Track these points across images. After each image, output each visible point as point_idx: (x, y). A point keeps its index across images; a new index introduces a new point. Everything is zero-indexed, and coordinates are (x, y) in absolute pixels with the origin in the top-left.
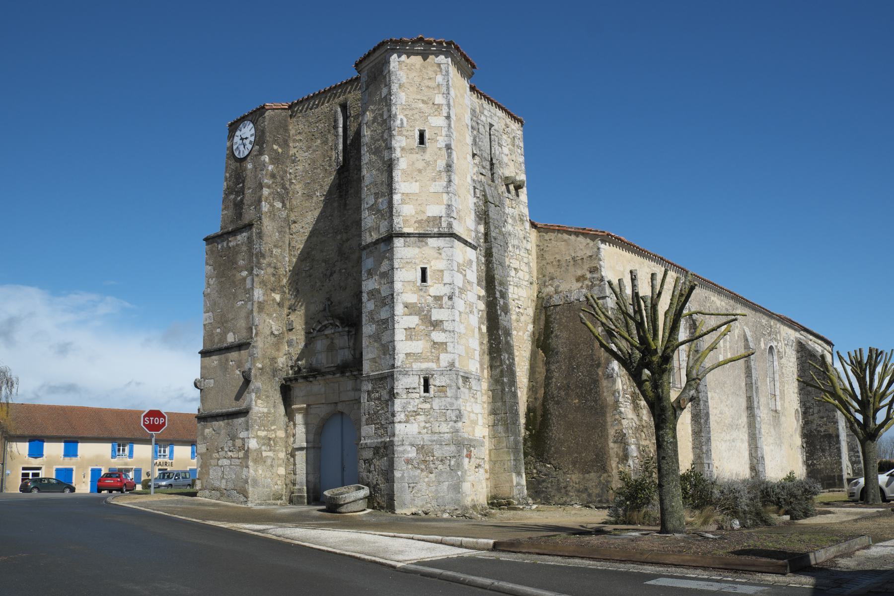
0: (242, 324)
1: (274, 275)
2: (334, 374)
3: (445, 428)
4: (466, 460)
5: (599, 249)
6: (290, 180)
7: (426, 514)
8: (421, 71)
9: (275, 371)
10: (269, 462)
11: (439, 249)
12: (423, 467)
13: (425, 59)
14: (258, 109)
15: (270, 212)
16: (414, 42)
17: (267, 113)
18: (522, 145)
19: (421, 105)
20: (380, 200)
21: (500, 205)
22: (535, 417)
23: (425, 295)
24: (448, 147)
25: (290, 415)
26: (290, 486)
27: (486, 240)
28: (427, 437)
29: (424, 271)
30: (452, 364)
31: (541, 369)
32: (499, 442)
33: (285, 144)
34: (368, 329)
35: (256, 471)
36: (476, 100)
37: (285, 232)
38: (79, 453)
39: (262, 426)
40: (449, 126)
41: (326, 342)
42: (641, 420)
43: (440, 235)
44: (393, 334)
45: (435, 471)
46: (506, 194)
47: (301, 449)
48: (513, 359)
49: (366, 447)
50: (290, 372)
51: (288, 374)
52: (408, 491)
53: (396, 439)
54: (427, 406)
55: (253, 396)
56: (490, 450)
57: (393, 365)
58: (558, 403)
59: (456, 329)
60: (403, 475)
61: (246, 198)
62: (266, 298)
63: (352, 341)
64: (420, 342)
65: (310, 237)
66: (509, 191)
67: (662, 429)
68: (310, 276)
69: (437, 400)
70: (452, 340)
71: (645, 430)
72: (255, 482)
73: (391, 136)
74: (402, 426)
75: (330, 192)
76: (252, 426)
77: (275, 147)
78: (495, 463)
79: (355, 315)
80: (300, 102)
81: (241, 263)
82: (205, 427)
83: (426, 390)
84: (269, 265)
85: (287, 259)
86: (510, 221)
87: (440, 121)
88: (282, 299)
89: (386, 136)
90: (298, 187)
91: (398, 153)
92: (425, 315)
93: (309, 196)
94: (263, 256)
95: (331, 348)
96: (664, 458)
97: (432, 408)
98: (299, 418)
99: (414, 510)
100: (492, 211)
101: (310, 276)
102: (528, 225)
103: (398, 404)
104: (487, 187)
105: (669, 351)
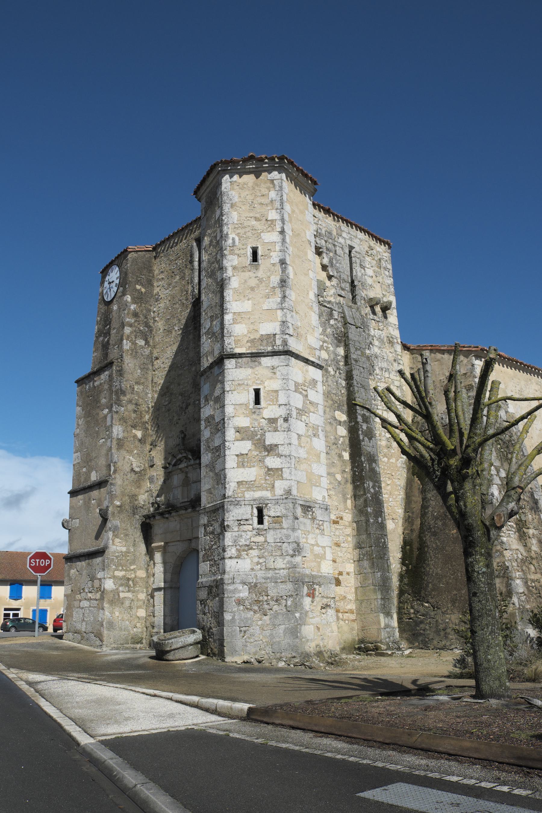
0: (102, 461)
1: (135, 411)
2: (186, 509)
3: (280, 563)
4: (307, 601)
5: (473, 365)
6: (154, 318)
7: (259, 662)
8: (254, 189)
9: (135, 509)
10: (127, 603)
11: (273, 368)
12: (256, 608)
13: (257, 177)
14: (122, 253)
15: (132, 350)
16: (245, 161)
17: (130, 256)
18: (390, 266)
19: (254, 222)
20: (214, 323)
21: (363, 326)
22: (411, 550)
23: (258, 418)
24: (283, 262)
25: (150, 552)
26: (150, 628)
27: (346, 363)
28: (260, 574)
29: (257, 392)
30: (289, 492)
31: (417, 498)
32: (365, 579)
33: (149, 284)
34: (206, 458)
35: (112, 613)
36: (333, 223)
37: (148, 369)
38: (53, 595)
39: (120, 566)
40: (284, 241)
41: (181, 476)
42: (529, 550)
43: (275, 353)
44: (224, 462)
45: (269, 613)
46: (372, 316)
47: (159, 589)
48: (380, 487)
50: (152, 509)
51: (149, 511)
52: (239, 636)
53: (226, 576)
54: (261, 539)
55: (110, 534)
56: (356, 589)
57: (225, 495)
58: (435, 534)
59: (293, 454)
60: (233, 618)
61: (112, 339)
62: (126, 434)
64: (252, 469)
65: (169, 371)
66: (374, 313)
67: (471, 555)
68: (169, 410)
69: (272, 532)
70: (289, 465)
71: (534, 562)
72: (111, 625)
73: (223, 256)
74: (234, 561)
75: (186, 325)
76: (109, 566)
77: (138, 287)
78: (362, 602)
80: (163, 242)
81: (104, 401)
82: (71, 568)
83: (261, 521)
84: (130, 401)
85: (150, 395)
86: (376, 343)
87: (273, 237)
88: (144, 436)
89: (219, 257)
90: (160, 325)
91: (229, 272)
92: (259, 439)
93: (169, 332)
94: (123, 393)
96: (475, 594)
97: (266, 541)
98: (158, 557)
99: (246, 658)
100: (353, 333)
101: (169, 410)
102: (399, 348)
103: (229, 537)
104: (346, 309)
105: (470, 450)
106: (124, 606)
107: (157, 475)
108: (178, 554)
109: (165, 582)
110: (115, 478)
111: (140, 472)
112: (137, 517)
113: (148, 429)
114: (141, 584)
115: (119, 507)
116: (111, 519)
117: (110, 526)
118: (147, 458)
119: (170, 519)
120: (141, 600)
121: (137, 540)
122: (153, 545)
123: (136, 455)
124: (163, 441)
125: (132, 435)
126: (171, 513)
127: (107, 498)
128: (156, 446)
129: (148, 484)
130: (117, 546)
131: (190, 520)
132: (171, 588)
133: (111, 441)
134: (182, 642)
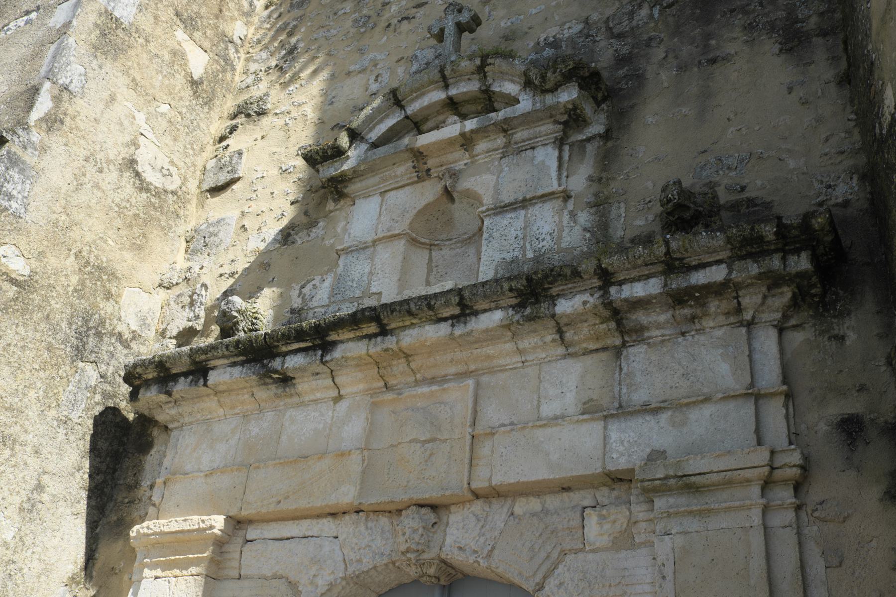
9: (88, 335)
110: (43, 149)
111: (162, 193)
112: (91, 374)
113: (233, 69)
118: (200, 164)
119: (303, 385)
121: (53, 487)
124: (324, 75)
125: (171, 43)
126: (327, 347)
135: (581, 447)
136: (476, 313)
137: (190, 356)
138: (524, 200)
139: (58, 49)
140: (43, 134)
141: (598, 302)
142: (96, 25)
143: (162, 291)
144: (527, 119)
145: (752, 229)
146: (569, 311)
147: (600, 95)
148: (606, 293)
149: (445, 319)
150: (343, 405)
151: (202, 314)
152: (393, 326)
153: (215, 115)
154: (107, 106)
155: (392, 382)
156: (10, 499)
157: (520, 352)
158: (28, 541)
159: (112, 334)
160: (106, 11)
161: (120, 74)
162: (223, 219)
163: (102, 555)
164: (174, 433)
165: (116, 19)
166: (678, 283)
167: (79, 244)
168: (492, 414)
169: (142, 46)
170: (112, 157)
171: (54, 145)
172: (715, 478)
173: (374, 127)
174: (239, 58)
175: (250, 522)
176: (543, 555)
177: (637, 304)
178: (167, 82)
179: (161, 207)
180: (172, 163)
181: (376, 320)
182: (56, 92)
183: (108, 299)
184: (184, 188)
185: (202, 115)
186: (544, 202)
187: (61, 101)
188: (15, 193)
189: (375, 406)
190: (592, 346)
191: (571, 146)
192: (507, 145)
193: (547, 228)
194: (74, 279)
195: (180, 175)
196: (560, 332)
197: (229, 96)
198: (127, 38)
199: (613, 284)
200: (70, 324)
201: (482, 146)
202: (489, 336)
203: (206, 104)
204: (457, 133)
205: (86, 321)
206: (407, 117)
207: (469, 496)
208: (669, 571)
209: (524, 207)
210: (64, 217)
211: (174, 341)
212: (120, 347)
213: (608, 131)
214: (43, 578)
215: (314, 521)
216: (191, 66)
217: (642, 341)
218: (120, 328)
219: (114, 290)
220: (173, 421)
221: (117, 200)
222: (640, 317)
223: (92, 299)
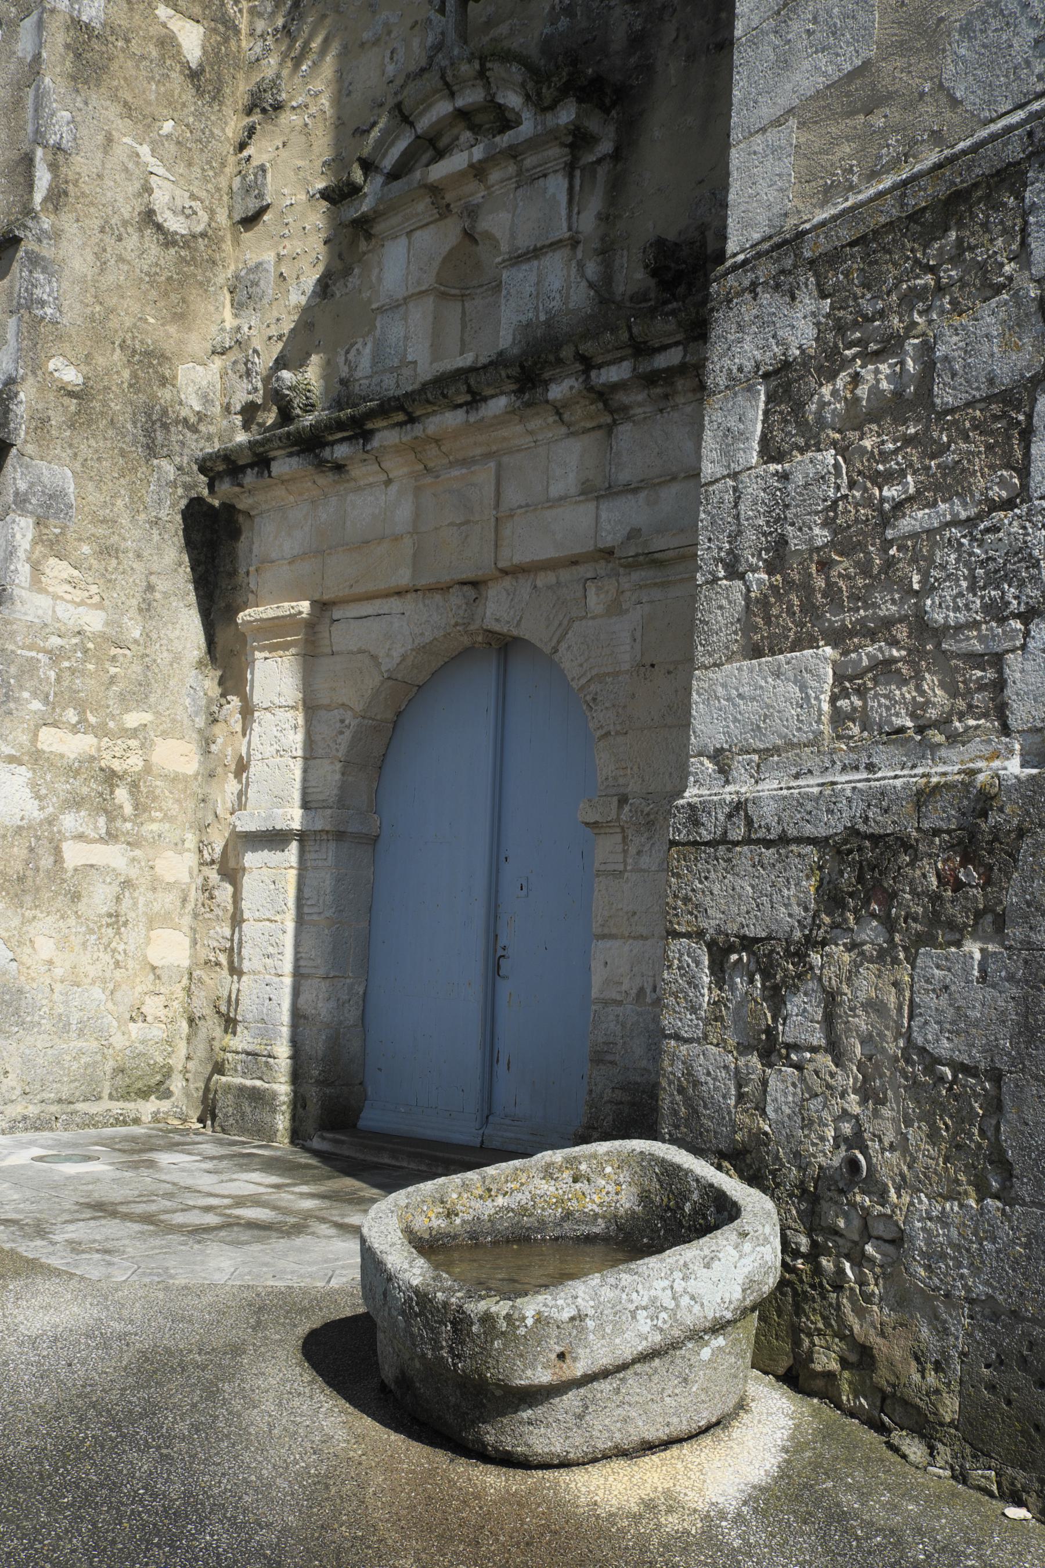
2: (476, 400)
9: (156, 427)
10: (99, 897)
25: (226, 654)
26: (212, 1027)
39: (65, 702)
41: (436, 240)
47: (273, 839)
49: (748, 833)
63: (595, 204)
79: (618, 38)
95: (463, 277)
98: (275, 677)
106: (82, 907)
107: (279, 258)
108: (387, 664)
109: (305, 805)
110: (56, 235)
111: (189, 241)
112: (168, 469)
113: (237, 31)
114: (175, 809)
115: (71, 394)
116: (30, 449)
117: (22, 486)
118: (224, 185)
119: (356, 471)
120: (169, 886)
121: (162, 585)
122: (242, 617)
123: (172, 148)
125: (155, 30)
126: (367, 435)
127: (10, 335)
128: (278, 107)
129: (228, 313)
130: (56, 597)
131: (485, 475)
132: (340, 836)
133: (40, 25)
134: (654, 1306)
135: (576, 526)
136: (485, 399)
137: (250, 449)
138: (535, 249)
139: (37, 97)
140: (52, 216)
141: (582, 387)
142: (67, 46)
143: (216, 358)
144: (533, 144)
145: (697, 313)
146: (559, 396)
147: (607, 101)
148: (588, 377)
149: (460, 406)
150: (394, 488)
151: (260, 385)
152: (418, 413)
153: (228, 111)
154: (106, 152)
155: (431, 465)
156: (128, 603)
157: (531, 433)
158: (154, 636)
159: (177, 422)
160: (72, 18)
161: (109, 102)
162: (261, 264)
163: (220, 639)
164: (257, 520)
165: (87, 25)
166: (645, 367)
167: (120, 333)
168: (513, 496)
169: (123, 50)
170: (127, 216)
171: (66, 225)
172: (671, 554)
173: (387, 151)
174: (240, 11)
175: (334, 603)
176: (556, 623)
177: (615, 387)
178: (162, 89)
179: (193, 258)
180: (193, 197)
181: (403, 408)
182: (50, 157)
183: (164, 385)
184: (213, 224)
185: (213, 118)
186: (554, 251)
187: (58, 167)
188: (45, 297)
189: (418, 490)
190: (589, 425)
191: (583, 169)
192: (520, 173)
193: (557, 285)
194: (126, 374)
195: (205, 209)
196: (559, 414)
197: (240, 75)
198: (104, 49)
199: (594, 367)
200: (134, 423)
201: (495, 176)
202: (499, 421)
203: (214, 99)
204: (465, 165)
205: (149, 416)
206: (418, 137)
207: (498, 574)
208: (638, 635)
209: (536, 257)
210: (98, 308)
211: (240, 417)
212: (189, 434)
213: (617, 149)
214: (175, 665)
215: (384, 601)
216: (185, 52)
217: (629, 418)
218: (184, 412)
219: (167, 373)
220: (253, 508)
221: (146, 268)
222: (622, 398)
223: (149, 390)
